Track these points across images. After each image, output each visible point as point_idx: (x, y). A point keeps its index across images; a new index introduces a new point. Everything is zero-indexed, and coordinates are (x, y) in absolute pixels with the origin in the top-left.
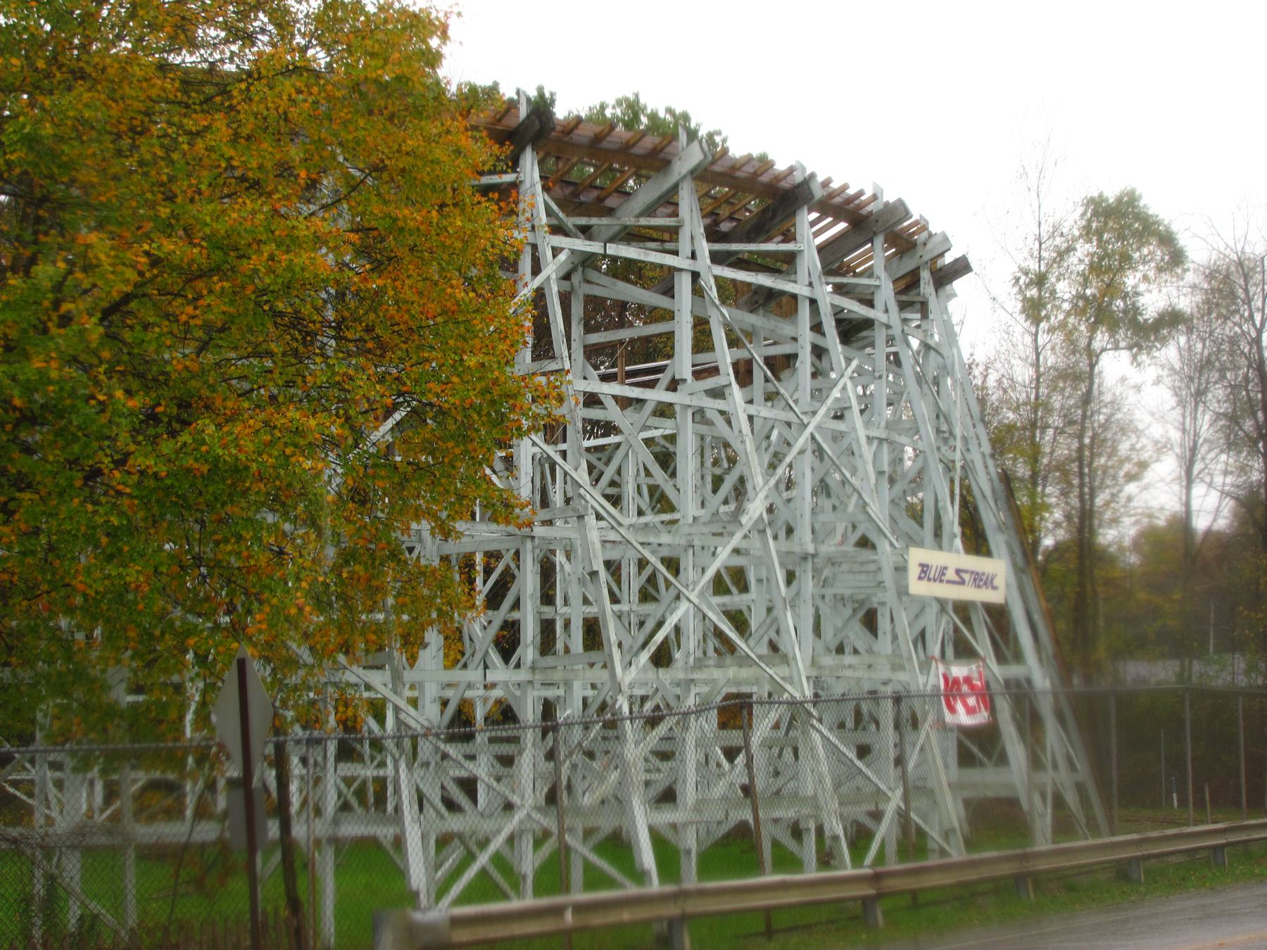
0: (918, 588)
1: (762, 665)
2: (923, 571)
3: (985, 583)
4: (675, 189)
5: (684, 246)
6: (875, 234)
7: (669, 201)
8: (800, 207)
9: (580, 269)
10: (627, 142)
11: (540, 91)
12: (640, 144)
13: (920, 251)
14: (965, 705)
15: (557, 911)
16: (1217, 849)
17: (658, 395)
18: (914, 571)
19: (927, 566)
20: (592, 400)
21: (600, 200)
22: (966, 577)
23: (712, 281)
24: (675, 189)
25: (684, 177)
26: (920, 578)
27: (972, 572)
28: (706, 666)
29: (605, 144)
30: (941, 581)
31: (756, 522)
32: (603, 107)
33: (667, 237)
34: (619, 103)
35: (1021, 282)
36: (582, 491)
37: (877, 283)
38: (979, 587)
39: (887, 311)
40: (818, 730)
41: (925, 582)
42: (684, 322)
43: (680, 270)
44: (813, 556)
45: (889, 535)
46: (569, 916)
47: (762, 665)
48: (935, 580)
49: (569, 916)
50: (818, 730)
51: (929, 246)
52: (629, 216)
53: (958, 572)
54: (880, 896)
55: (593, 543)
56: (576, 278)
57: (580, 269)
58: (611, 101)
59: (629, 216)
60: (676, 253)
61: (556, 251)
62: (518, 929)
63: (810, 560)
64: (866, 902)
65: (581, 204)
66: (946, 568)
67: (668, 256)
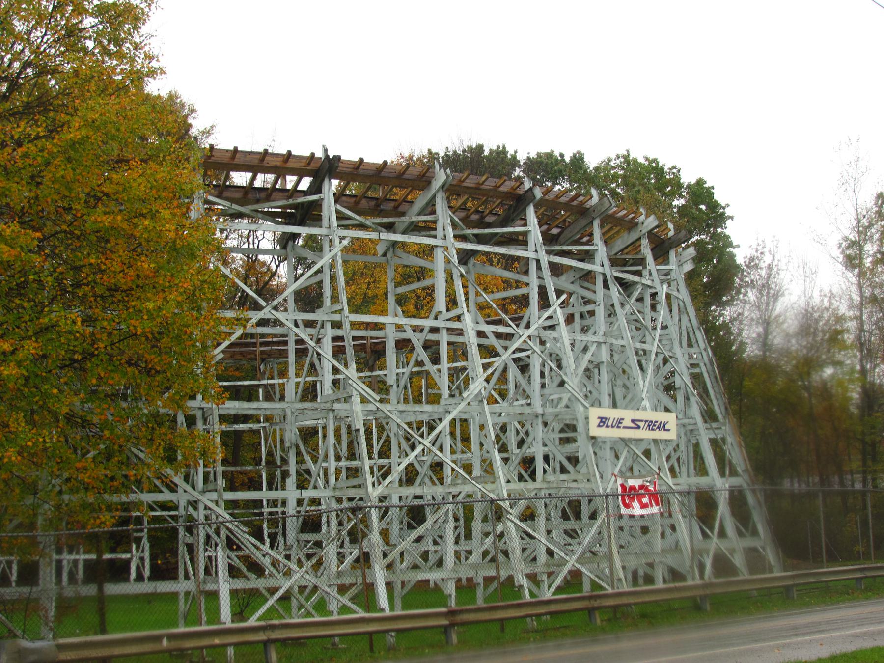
0: (595, 431)
1: (473, 482)
2: (601, 422)
3: (659, 428)
4: (434, 197)
5: (440, 233)
6: (594, 219)
7: (432, 203)
8: (529, 204)
9: (391, 250)
10: (399, 173)
11: (429, 151)
12: (407, 172)
13: (640, 228)
14: (640, 502)
15: (158, 639)
16: (788, 589)
17: (428, 323)
18: (594, 422)
19: (606, 419)
20: (400, 328)
21: (396, 208)
22: (641, 424)
23: (454, 252)
24: (434, 197)
25: (438, 190)
26: (599, 426)
27: (646, 421)
28: (458, 484)
29: (383, 174)
30: (618, 427)
31: (477, 396)
32: (610, 160)
33: (428, 228)
34: (618, 157)
35: (843, 245)
36: (350, 382)
37: (595, 248)
38: (653, 430)
39: (602, 265)
40: (512, 521)
41: (604, 428)
42: (439, 277)
43: (437, 246)
44: (543, 415)
45: (582, 401)
46: (165, 642)
47: (473, 482)
48: (612, 427)
49: (165, 642)
50: (512, 521)
51: (645, 224)
52: (413, 216)
53: (633, 421)
54: (452, 625)
55: (357, 412)
56: (389, 255)
57: (391, 250)
58: (613, 156)
59: (413, 216)
60: (435, 237)
61: (342, 238)
62: (117, 651)
63: (540, 417)
64: (446, 629)
65: (381, 210)
66: (623, 419)
67: (425, 238)
